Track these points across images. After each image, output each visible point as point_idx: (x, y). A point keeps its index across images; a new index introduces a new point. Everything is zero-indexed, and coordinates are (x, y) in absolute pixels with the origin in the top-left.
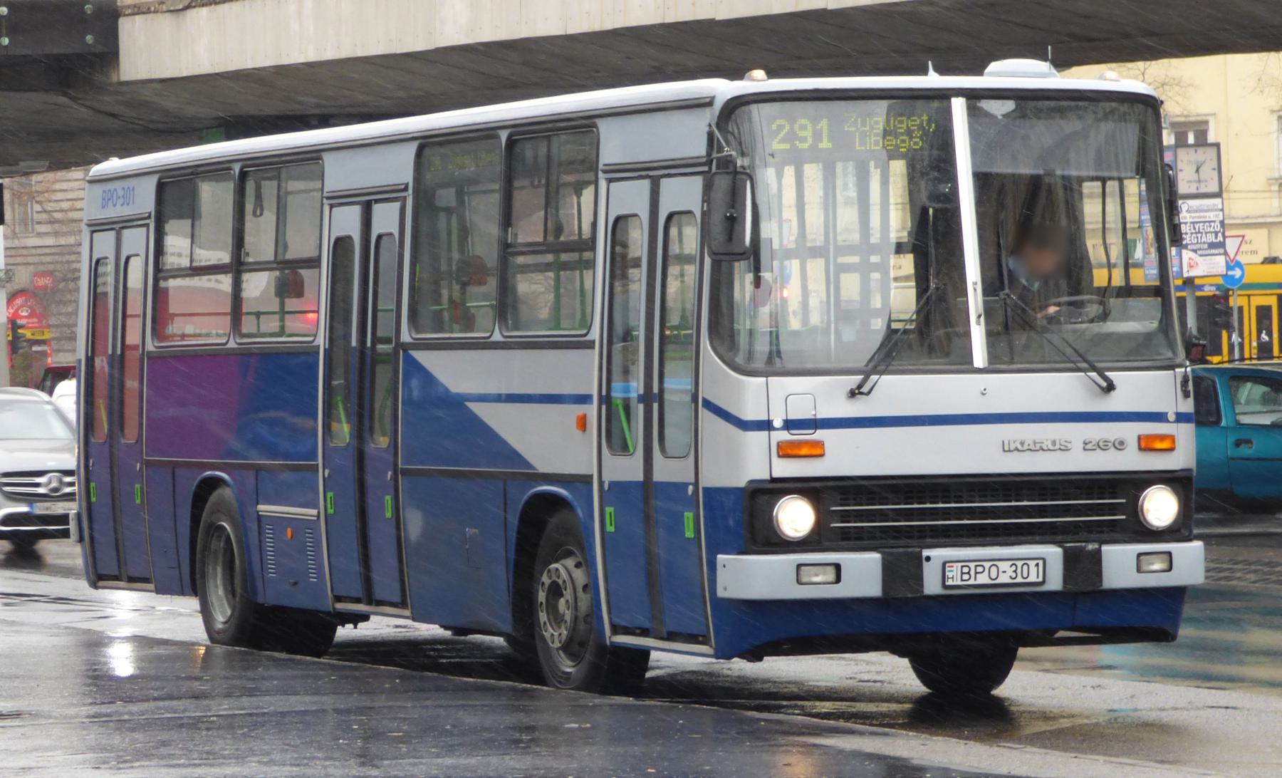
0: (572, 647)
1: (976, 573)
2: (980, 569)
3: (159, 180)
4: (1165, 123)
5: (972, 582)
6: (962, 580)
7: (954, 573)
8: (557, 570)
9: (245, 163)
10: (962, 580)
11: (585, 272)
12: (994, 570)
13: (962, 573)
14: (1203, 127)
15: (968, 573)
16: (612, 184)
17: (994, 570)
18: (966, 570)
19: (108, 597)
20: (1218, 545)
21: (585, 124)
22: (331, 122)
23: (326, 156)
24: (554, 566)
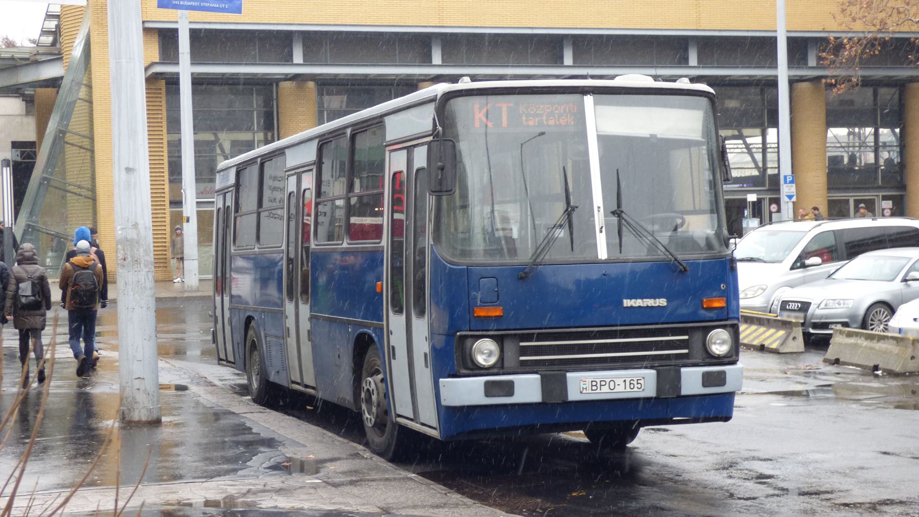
0: (380, 425)
1: (601, 385)
2: (603, 383)
3: (237, 169)
4: (344, 182)
5: (598, 391)
6: (592, 390)
7: (587, 385)
8: (370, 382)
9: (263, 158)
10: (592, 390)
11: (69, 345)
12: (612, 383)
13: (592, 386)
14: (203, 186)
15: (596, 385)
16: (392, 153)
17: (612, 383)
18: (594, 383)
19: (67, 471)
20: (711, 201)
21: (378, 122)
22: (592, 89)
23: (287, 151)
24: (369, 379)
